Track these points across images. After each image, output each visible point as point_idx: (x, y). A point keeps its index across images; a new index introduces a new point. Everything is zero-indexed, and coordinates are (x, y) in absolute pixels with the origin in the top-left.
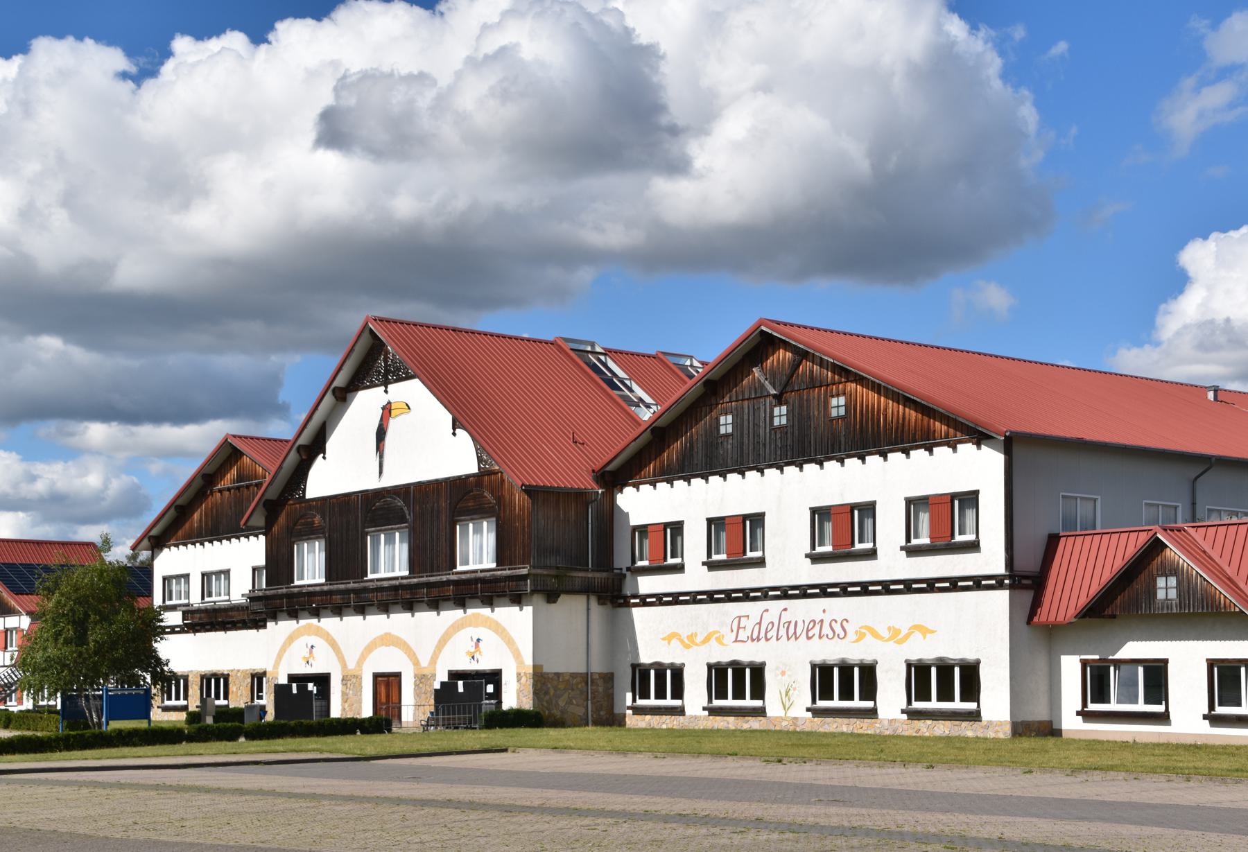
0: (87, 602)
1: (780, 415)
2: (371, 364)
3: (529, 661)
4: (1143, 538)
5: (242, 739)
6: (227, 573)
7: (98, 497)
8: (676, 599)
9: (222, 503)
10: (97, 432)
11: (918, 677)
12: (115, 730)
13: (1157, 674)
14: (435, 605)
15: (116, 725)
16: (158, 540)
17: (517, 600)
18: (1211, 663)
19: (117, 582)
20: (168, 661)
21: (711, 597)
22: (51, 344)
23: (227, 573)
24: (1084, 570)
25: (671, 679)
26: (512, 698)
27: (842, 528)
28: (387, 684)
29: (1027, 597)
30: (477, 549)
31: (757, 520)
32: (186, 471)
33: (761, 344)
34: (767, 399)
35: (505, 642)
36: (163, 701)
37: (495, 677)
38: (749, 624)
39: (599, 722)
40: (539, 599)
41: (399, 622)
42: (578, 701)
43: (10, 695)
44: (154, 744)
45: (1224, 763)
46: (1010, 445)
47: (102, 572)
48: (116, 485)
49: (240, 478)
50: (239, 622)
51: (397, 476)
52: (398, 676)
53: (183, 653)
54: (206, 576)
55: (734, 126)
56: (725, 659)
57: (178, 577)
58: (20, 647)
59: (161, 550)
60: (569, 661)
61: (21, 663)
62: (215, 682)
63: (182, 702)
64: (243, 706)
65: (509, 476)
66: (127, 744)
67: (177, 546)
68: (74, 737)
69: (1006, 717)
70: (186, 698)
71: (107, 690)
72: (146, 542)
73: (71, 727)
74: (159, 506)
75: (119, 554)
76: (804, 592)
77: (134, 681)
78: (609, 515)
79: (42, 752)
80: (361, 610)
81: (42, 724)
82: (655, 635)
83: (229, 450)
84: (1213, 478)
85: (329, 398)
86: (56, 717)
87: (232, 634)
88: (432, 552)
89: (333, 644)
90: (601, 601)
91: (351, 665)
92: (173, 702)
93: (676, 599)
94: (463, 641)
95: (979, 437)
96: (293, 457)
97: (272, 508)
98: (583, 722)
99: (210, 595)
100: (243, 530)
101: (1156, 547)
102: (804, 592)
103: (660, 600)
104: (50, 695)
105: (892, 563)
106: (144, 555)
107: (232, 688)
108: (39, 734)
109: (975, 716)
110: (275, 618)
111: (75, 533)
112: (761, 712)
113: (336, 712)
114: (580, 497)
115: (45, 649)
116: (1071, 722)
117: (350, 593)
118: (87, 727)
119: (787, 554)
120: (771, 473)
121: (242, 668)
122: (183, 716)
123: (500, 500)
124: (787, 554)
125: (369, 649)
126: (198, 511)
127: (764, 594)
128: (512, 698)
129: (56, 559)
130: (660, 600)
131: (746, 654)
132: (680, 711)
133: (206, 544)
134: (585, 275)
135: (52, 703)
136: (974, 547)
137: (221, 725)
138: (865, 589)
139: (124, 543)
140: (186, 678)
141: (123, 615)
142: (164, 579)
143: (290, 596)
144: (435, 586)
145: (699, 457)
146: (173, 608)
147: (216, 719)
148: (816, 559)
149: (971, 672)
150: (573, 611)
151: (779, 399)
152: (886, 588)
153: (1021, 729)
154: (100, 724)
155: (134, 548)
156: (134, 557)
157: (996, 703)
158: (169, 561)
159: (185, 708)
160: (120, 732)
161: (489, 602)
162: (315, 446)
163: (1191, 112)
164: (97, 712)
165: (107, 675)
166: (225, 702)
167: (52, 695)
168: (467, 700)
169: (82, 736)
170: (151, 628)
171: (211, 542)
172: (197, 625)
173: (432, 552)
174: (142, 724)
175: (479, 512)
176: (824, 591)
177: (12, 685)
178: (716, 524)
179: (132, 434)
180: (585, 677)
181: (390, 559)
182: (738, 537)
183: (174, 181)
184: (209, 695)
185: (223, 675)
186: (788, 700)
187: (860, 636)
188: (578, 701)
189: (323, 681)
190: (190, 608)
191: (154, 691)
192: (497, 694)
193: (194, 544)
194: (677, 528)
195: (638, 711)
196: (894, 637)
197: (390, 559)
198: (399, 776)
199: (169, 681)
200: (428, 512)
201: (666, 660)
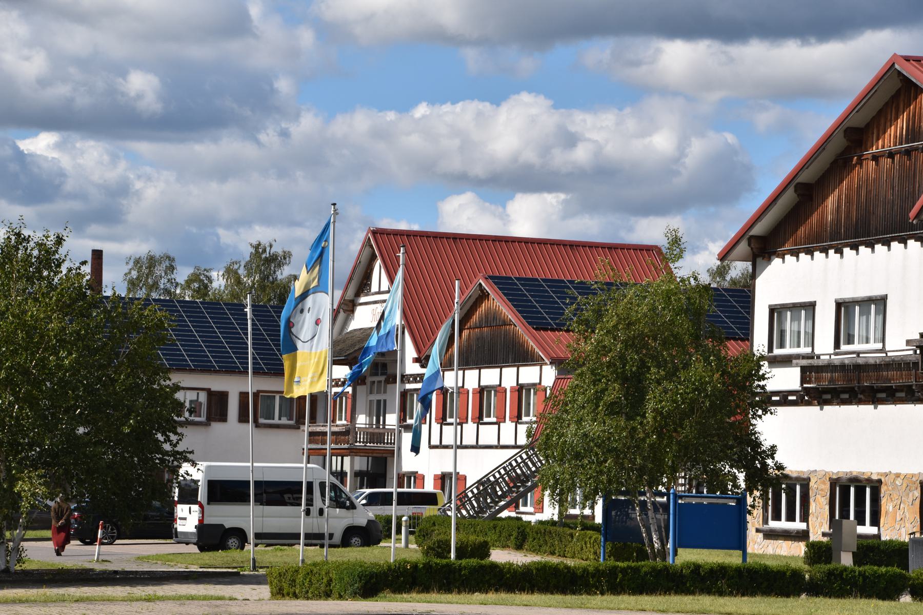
0: (646, 345)
5: (906, 599)
6: (881, 302)
7: (669, 167)
9: (877, 180)
12: (687, 565)
15: (688, 556)
16: (763, 245)
19: (693, 312)
20: (773, 449)
23: (881, 302)
32: (818, 124)
36: (765, 521)
43: (524, 495)
44: (753, 594)
47: (668, 295)
48: (698, 149)
50: (900, 389)
53: (802, 440)
54: (843, 308)
57: (795, 307)
58: (541, 417)
59: (769, 261)
61: (540, 442)
62: (856, 494)
63: (798, 525)
64: (906, 538)
66: (708, 591)
67: (795, 253)
68: (624, 570)
70: (805, 518)
71: (677, 497)
72: (743, 247)
73: (617, 554)
74: (768, 182)
75: (699, 264)
77: (717, 482)
79: (574, 593)
81: (575, 545)
83: (898, 84)
86: (595, 535)
87: (887, 410)
92: (783, 524)
99: (850, 340)
100: (912, 227)
104: (586, 498)
106: (739, 268)
107: (887, 505)
108: (570, 562)
111: (631, 229)
115: (579, 422)
118: (643, 555)
121: (904, 471)
122: (799, 549)
129: (598, 272)
133: (847, 251)
135: (587, 512)
137: (868, 569)
139: (706, 248)
140: (805, 483)
141: (697, 369)
142: (773, 310)
146: (786, 361)
147: (858, 558)
154: (663, 554)
155: (723, 257)
156: (721, 272)
158: (781, 281)
159: (802, 536)
160: (696, 568)
164: (659, 530)
165: (674, 470)
166: (874, 530)
167: (589, 498)
169: (636, 570)
170: (743, 394)
171: (855, 247)
172: (826, 391)
174: (732, 558)
177: (528, 478)
179: (731, 60)
184: (845, 514)
185: (869, 480)
190: (814, 362)
191: (749, 500)
193: (825, 250)
195: (771, 535)
199: (787, 492)
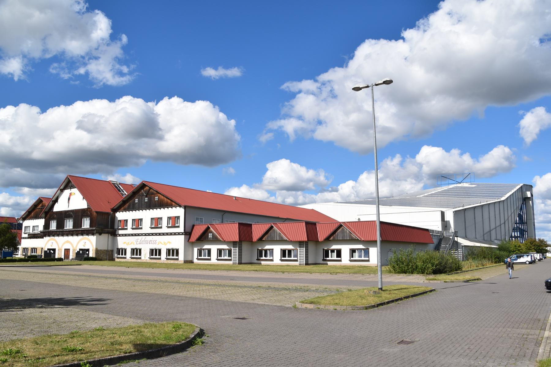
1: (146, 200)
2: (68, 184)
3: (95, 247)
4: (206, 226)
6: (38, 226)
8: (126, 235)
10: (26, 190)
11: (168, 251)
13: (209, 251)
14: (77, 235)
16: (24, 219)
17: (93, 234)
18: (218, 249)
21: (132, 235)
22: (19, 170)
23: (38, 226)
24: (198, 231)
25: (124, 251)
26: (91, 255)
27: (156, 222)
28: (67, 251)
29: (188, 236)
30: (86, 224)
31: (141, 220)
33: (143, 186)
34: (144, 196)
35: (90, 243)
37: (88, 250)
38: (139, 241)
39: (109, 260)
40: (97, 235)
41: (70, 238)
42: (106, 255)
45: (212, 267)
46: (185, 208)
49: (42, 206)
51: (70, 209)
52: (69, 249)
55: (176, 131)
56: (134, 248)
60: (104, 247)
62: (34, 249)
65: (93, 210)
69: (183, 259)
76: (149, 235)
78: (114, 218)
80: (63, 235)
82: (122, 242)
84: (226, 215)
85: (59, 191)
88: (77, 224)
89: (57, 242)
90: (111, 235)
91: (60, 247)
93: (126, 235)
94: (82, 243)
95: (180, 206)
96: (51, 203)
97: (46, 213)
98: (106, 260)
101: (208, 228)
102: (149, 235)
103: (123, 235)
105: (165, 230)
109: (178, 259)
110: (45, 236)
112: (140, 258)
113: (56, 257)
114: (108, 214)
116: (195, 261)
117: (61, 232)
119: (146, 227)
120: (144, 211)
123: (91, 214)
124: (146, 227)
125: (64, 243)
126: (32, 213)
127: (142, 235)
128: (91, 255)
130: (123, 235)
131: (138, 247)
132: (125, 258)
134: (144, 161)
136: (178, 227)
138: (160, 234)
143: (48, 232)
144: (77, 231)
145: (131, 207)
148: (152, 228)
149: (177, 251)
150: (105, 237)
151: (146, 196)
152: (163, 234)
153: (186, 262)
157: (181, 257)
158: (26, 223)
161: (88, 235)
162: (56, 201)
163: (265, 138)
168: (82, 255)
173: (77, 224)
175: (87, 216)
176: (152, 234)
178: (134, 220)
180: (107, 251)
181: (69, 225)
182: (138, 223)
183: (47, 135)
186: (145, 256)
187: (159, 244)
188: (106, 255)
189: (54, 250)
192: (88, 254)
194: (127, 221)
195: (118, 258)
196: (164, 243)
197: (69, 225)
198: (65, 269)
200: (77, 215)
201: (123, 247)
